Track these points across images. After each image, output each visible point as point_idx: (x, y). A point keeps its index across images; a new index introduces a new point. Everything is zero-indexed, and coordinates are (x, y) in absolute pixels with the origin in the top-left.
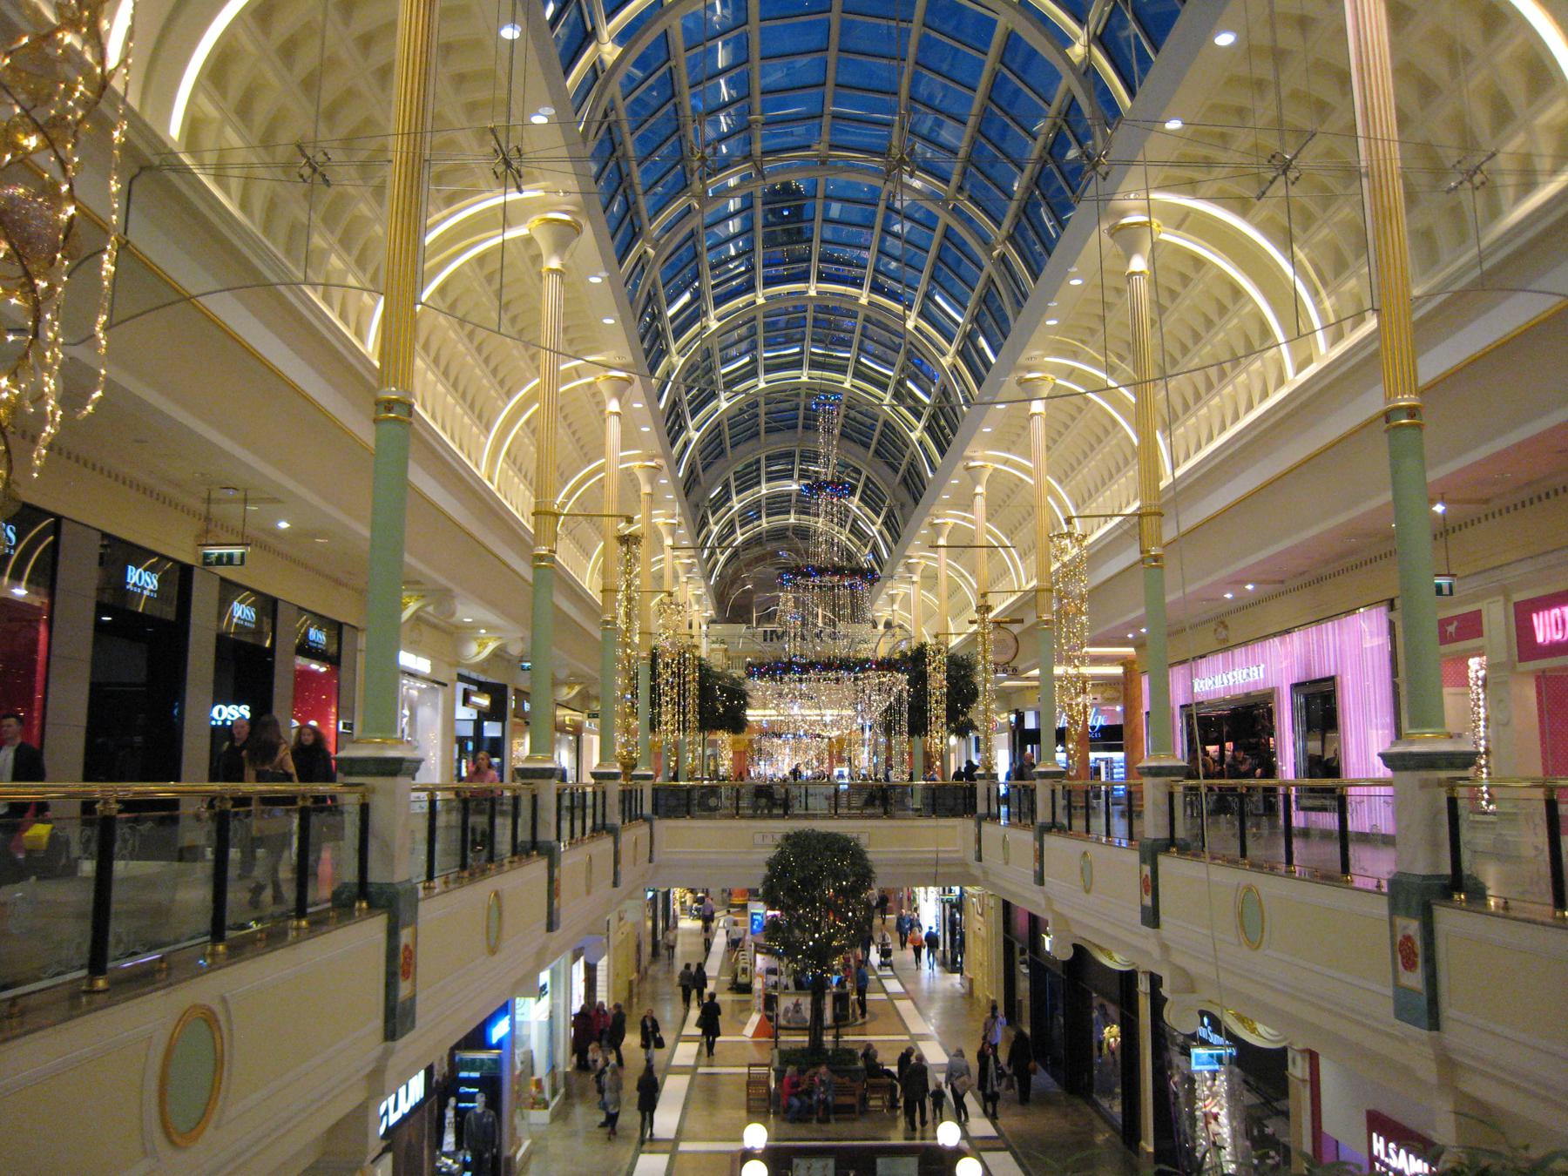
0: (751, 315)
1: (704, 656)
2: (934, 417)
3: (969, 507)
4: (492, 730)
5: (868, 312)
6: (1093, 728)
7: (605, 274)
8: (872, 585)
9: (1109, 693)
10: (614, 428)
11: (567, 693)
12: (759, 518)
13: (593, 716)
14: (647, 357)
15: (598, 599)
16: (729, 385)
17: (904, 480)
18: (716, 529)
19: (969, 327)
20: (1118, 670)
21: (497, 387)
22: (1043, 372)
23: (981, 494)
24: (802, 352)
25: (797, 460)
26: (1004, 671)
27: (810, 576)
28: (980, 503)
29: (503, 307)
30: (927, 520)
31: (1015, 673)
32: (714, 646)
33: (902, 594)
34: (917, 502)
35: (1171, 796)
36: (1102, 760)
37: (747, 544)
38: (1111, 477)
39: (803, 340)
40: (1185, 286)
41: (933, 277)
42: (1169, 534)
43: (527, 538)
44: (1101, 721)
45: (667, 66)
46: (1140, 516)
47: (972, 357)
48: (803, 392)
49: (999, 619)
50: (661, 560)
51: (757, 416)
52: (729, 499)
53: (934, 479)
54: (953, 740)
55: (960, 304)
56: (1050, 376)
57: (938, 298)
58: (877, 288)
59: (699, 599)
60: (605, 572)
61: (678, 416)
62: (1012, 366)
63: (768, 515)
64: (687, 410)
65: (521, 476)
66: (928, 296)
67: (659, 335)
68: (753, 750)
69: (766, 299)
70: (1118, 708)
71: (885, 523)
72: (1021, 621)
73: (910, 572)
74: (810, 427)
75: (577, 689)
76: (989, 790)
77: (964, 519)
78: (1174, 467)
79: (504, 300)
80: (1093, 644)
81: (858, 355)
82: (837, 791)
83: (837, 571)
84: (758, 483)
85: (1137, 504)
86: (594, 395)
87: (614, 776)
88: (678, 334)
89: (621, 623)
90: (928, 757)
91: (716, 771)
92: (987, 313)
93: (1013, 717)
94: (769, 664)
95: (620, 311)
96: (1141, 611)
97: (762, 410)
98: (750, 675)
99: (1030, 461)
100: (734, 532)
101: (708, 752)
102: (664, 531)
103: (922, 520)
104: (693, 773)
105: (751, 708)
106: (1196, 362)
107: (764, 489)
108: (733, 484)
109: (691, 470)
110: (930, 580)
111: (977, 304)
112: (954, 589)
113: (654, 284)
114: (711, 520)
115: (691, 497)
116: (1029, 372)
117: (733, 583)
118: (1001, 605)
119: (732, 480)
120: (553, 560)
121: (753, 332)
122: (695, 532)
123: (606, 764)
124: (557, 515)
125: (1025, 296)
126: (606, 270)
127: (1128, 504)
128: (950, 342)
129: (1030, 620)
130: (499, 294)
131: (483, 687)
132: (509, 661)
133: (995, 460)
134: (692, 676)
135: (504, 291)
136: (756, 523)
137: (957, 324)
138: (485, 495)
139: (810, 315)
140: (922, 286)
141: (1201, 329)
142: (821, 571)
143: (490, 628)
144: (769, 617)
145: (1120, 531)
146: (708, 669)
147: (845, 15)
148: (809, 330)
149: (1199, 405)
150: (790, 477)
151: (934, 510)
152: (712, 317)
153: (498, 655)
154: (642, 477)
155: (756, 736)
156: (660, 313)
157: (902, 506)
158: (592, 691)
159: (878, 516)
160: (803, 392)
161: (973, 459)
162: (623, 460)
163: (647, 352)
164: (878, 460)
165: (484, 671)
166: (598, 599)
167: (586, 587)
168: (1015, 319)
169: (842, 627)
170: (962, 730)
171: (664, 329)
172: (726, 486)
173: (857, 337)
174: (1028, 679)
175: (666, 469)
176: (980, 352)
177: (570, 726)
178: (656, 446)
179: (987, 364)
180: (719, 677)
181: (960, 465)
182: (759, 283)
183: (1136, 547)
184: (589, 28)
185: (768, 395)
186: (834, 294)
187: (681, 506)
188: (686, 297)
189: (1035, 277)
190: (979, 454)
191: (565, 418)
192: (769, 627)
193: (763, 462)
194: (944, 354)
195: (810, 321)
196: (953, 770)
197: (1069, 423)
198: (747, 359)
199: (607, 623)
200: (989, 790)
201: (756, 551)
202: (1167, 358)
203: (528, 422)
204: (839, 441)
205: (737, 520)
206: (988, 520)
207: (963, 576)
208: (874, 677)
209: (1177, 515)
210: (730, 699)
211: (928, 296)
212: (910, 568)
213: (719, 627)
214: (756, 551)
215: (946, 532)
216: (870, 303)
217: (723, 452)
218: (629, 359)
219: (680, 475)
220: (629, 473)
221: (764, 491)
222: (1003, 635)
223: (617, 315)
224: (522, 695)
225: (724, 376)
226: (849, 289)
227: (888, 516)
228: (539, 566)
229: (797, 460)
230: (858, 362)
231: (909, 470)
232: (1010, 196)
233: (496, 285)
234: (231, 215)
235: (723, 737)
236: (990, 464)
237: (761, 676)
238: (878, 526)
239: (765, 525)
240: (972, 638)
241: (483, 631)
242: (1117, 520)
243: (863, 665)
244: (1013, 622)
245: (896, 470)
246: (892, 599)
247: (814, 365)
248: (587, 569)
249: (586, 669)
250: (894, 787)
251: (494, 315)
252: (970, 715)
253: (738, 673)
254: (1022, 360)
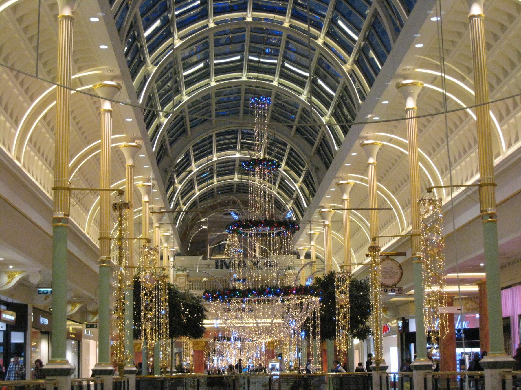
0: (205, 35)
1: (172, 282)
2: (338, 106)
3: (364, 172)
4: (17, 338)
5: (290, 33)
6: (459, 330)
7: (101, 14)
8: (294, 233)
9: (470, 305)
10: (107, 121)
11: (72, 310)
12: (212, 178)
13: (90, 326)
14: (129, 67)
15: (50, 195)
16: (188, 84)
17: (318, 150)
18: (180, 187)
19: (363, 43)
20: (475, 288)
21: (50, 131)
22: (415, 79)
23: (373, 164)
24: (241, 60)
25: (239, 136)
26: (393, 291)
27: (249, 227)
28: (372, 171)
29: (39, 56)
30: (334, 182)
31: (400, 292)
32: (180, 273)
33: (317, 233)
34: (327, 167)
35: (425, 379)
36: (467, 354)
37: (202, 198)
38: (465, 152)
39: (243, 51)
40: (511, 22)
41: (336, 8)
42: (500, 197)
43: (96, 251)
44: (465, 325)
45: (182, 121)
46: (480, 186)
47: (365, 64)
48: (243, 88)
49: (388, 252)
50: (140, 211)
51: (210, 105)
52: (189, 165)
53: (339, 151)
54: (356, 341)
55: (357, 29)
56: (420, 82)
57: (340, 23)
58: (295, 15)
59: (167, 238)
60: (102, 224)
61: (152, 106)
62: (393, 75)
63: (218, 176)
64: (146, 46)
65: (36, 151)
66: (333, 21)
67: (138, 51)
68: (209, 349)
69: (216, 23)
70: (478, 316)
71: (304, 181)
72: (404, 254)
73: (323, 218)
74: (248, 112)
75: (78, 306)
76: (381, 378)
77: (362, 180)
78: (509, 145)
79: (40, 52)
80: (454, 271)
81: (283, 61)
82: (270, 380)
83: (268, 223)
84: (211, 153)
85: (477, 177)
86: (119, 155)
87: (110, 373)
88: (152, 50)
89: (114, 262)
90: (337, 352)
91: (181, 365)
92: (375, 34)
93: (400, 324)
94: (220, 291)
95: (112, 40)
96: (482, 251)
97: (214, 100)
98: (207, 299)
99: (406, 139)
100: (193, 188)
101: (175, 350)
102: (142, 191)
103: (331, 180)
104: (165, 368)
105: (205, 319)
106: (498, 96)
107: (215, 157)
108: (192, 154)
109: (162, 147)
110: (338, 224)
111: (368, 28)
112: (355, 230)
113: (135, 17)
114: (176, 181)
115: (161, 164)
116: (405, 79)
117: (192, 227)
118: (385, 246)
119: (191, 151)
120: (67, 221)
121: (206, 46)
122: (164, 190)
123: (103, 363)
124: (110, 239)
125: (315, 191)
126: (102, 12)
127: (472, 176)
128: (349, 54)
129: (409, 255)
130: (37, 48)
131: (10, 307)
132: (29, 287)
133: (425, 78)
134: (164, 296)
135: (40, 46)
136: (209, 182)
137: (354, 41)
138: (15, 171)
139: (247, 34)
140: (328, 14)
141: (508, 68)
142: (256, 224)
143: (16, 264)
144: (219, 249)
145: (465, 196)
146: (176, 293)
147: (252, 33)
148: (247, 44)
149: (509, 117)
150: (235, 148)
151: (339, 174)
152: (184, 93)
153: (23, 284)
154: (126, 154)
155: (211, 340)
156: (139, 35)
157: (317, 170)
158: (90, 308)
159: (299, 176)
160: (243, 88)
161: (367, 138)
162: (115, 141)
163: (130, 64)
164: (299, 136)
165: (11, 296)
166: (50, 195)
167: (85, 232)
168: (394, 42)
169: (274, 258)
170: (363, 335)
171: (141, 47)
172: (187, 155)
173: (282, 49)
174: (410, 295)
175: (144, 148)
176: (371, 62)
177: (72, 334)
178: (137, 133)
179: (376, 71)
180: (183, 297)
181: (358, 142)
182: (211, 12)
183: (478, 206)
184: (142, 59)
185: (219, 92)
186: (267, 19)
187: (154, 173)
188: (158, 23)
189: (409, 12)
190: (370, 135)
191: (74, 118)
192: (218, 257)
193: (214, 139)
194: (345, 62)
195: (247, 39)
196: (356, 365)
197: (506, 23)
198: (202, 65)
199: (104, 262)
200: (381, 378)
201: (210, 202)
202: (449, 130)
203: (45, 117)
204: (270, 121)
205: (195, 179)
206: (379, 181)
207: (362, 220)
208: (294, 300)
209: (453, 220)
210: (192, 313)
211: (333, 21)
212: (323, 215)
213: (182, 258)
214: (210, 202)
215: (349, 190)
216: (291, 26)
217: (184, 131)
218: (118, 72)
219: (154, 149)
220: (116, 151)
221: (215, 159)
222: (391, 264)
223: (110, 42)
224: (39, 312)
225: (186, 77)
226: (277, 16)
227: (306, 177)
228: (103, 266)
229: (239, 136)
230: (283, 66)
231: (321, 143)
232: (364, 17)
233: (35, 44)
234: (48, 197)
235: (188, 342)
236: (379, 142)
237: (214, 299)
238: (299, 184)
239: (216, 183)
240: (367, 268)
241: (11, 267)
242: (463, 188)
243: (287, 291)
244: (398, 254)
245: (312, 144)
246: (310, 237)
247: (252, 69)
248: (86, 219)
249: (85, 292)
250: (312, 377)
251: (33, 62)
252: (367, 324)
253: (198, 293)
254: (399, 71)
